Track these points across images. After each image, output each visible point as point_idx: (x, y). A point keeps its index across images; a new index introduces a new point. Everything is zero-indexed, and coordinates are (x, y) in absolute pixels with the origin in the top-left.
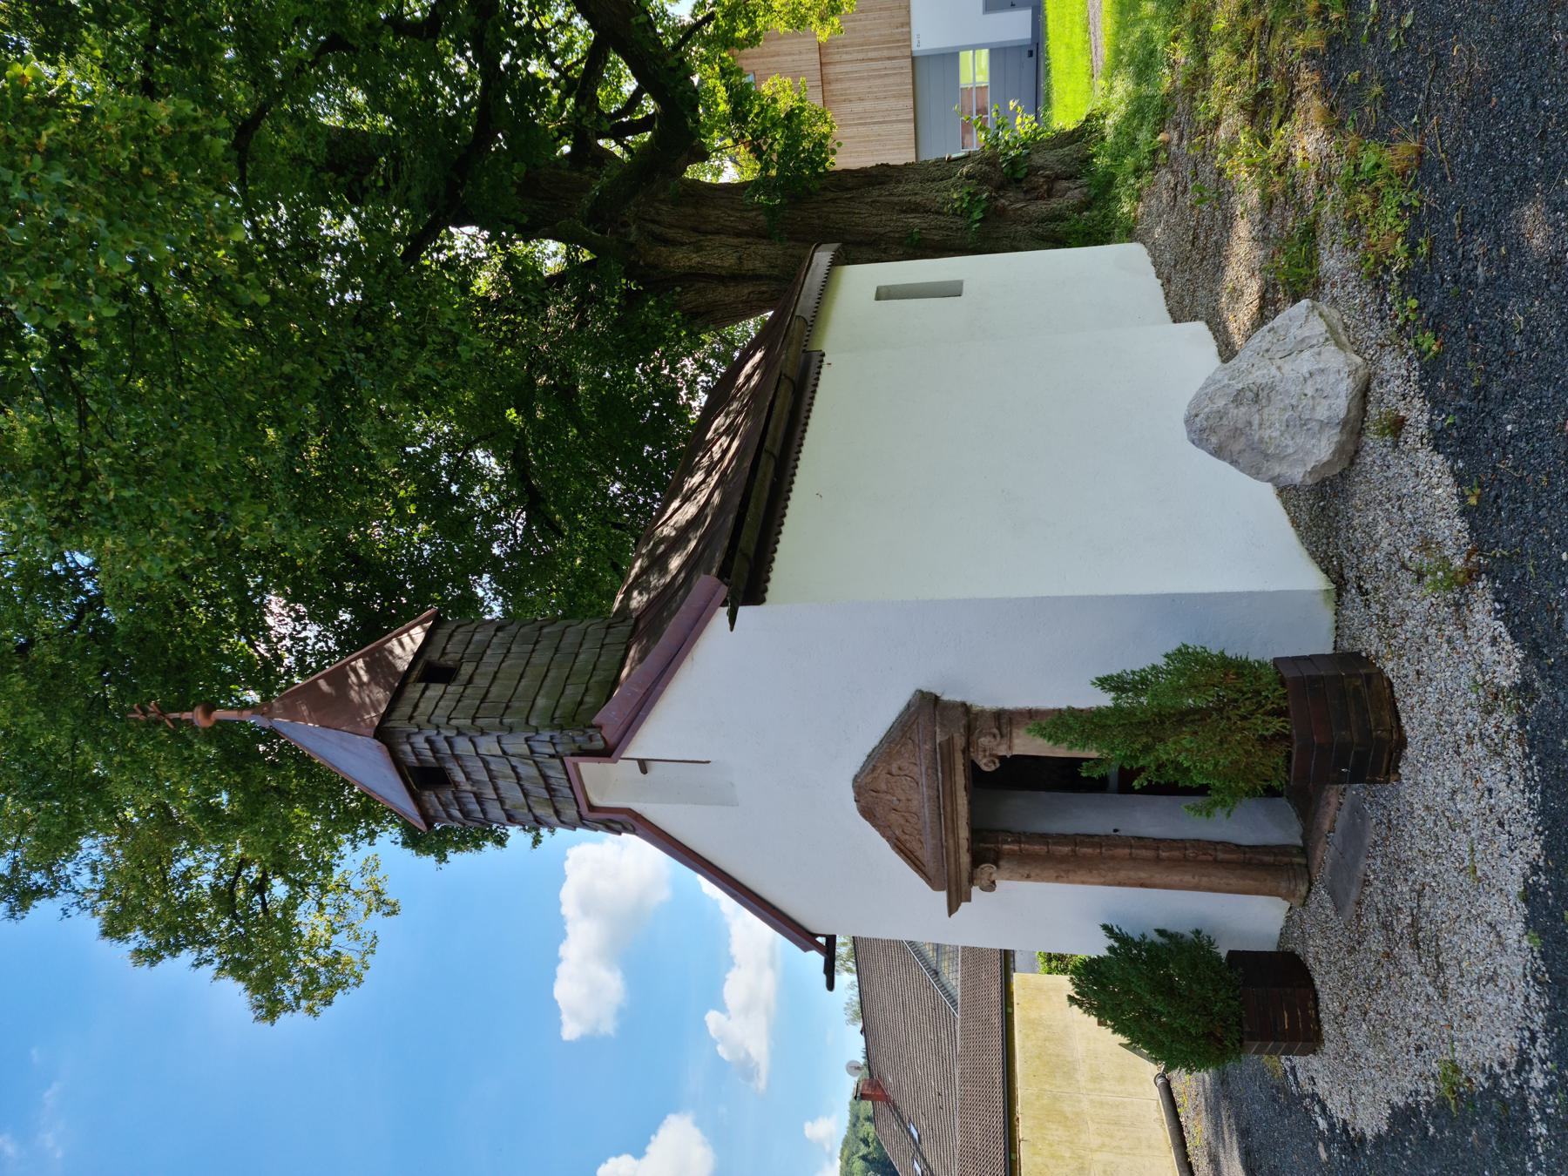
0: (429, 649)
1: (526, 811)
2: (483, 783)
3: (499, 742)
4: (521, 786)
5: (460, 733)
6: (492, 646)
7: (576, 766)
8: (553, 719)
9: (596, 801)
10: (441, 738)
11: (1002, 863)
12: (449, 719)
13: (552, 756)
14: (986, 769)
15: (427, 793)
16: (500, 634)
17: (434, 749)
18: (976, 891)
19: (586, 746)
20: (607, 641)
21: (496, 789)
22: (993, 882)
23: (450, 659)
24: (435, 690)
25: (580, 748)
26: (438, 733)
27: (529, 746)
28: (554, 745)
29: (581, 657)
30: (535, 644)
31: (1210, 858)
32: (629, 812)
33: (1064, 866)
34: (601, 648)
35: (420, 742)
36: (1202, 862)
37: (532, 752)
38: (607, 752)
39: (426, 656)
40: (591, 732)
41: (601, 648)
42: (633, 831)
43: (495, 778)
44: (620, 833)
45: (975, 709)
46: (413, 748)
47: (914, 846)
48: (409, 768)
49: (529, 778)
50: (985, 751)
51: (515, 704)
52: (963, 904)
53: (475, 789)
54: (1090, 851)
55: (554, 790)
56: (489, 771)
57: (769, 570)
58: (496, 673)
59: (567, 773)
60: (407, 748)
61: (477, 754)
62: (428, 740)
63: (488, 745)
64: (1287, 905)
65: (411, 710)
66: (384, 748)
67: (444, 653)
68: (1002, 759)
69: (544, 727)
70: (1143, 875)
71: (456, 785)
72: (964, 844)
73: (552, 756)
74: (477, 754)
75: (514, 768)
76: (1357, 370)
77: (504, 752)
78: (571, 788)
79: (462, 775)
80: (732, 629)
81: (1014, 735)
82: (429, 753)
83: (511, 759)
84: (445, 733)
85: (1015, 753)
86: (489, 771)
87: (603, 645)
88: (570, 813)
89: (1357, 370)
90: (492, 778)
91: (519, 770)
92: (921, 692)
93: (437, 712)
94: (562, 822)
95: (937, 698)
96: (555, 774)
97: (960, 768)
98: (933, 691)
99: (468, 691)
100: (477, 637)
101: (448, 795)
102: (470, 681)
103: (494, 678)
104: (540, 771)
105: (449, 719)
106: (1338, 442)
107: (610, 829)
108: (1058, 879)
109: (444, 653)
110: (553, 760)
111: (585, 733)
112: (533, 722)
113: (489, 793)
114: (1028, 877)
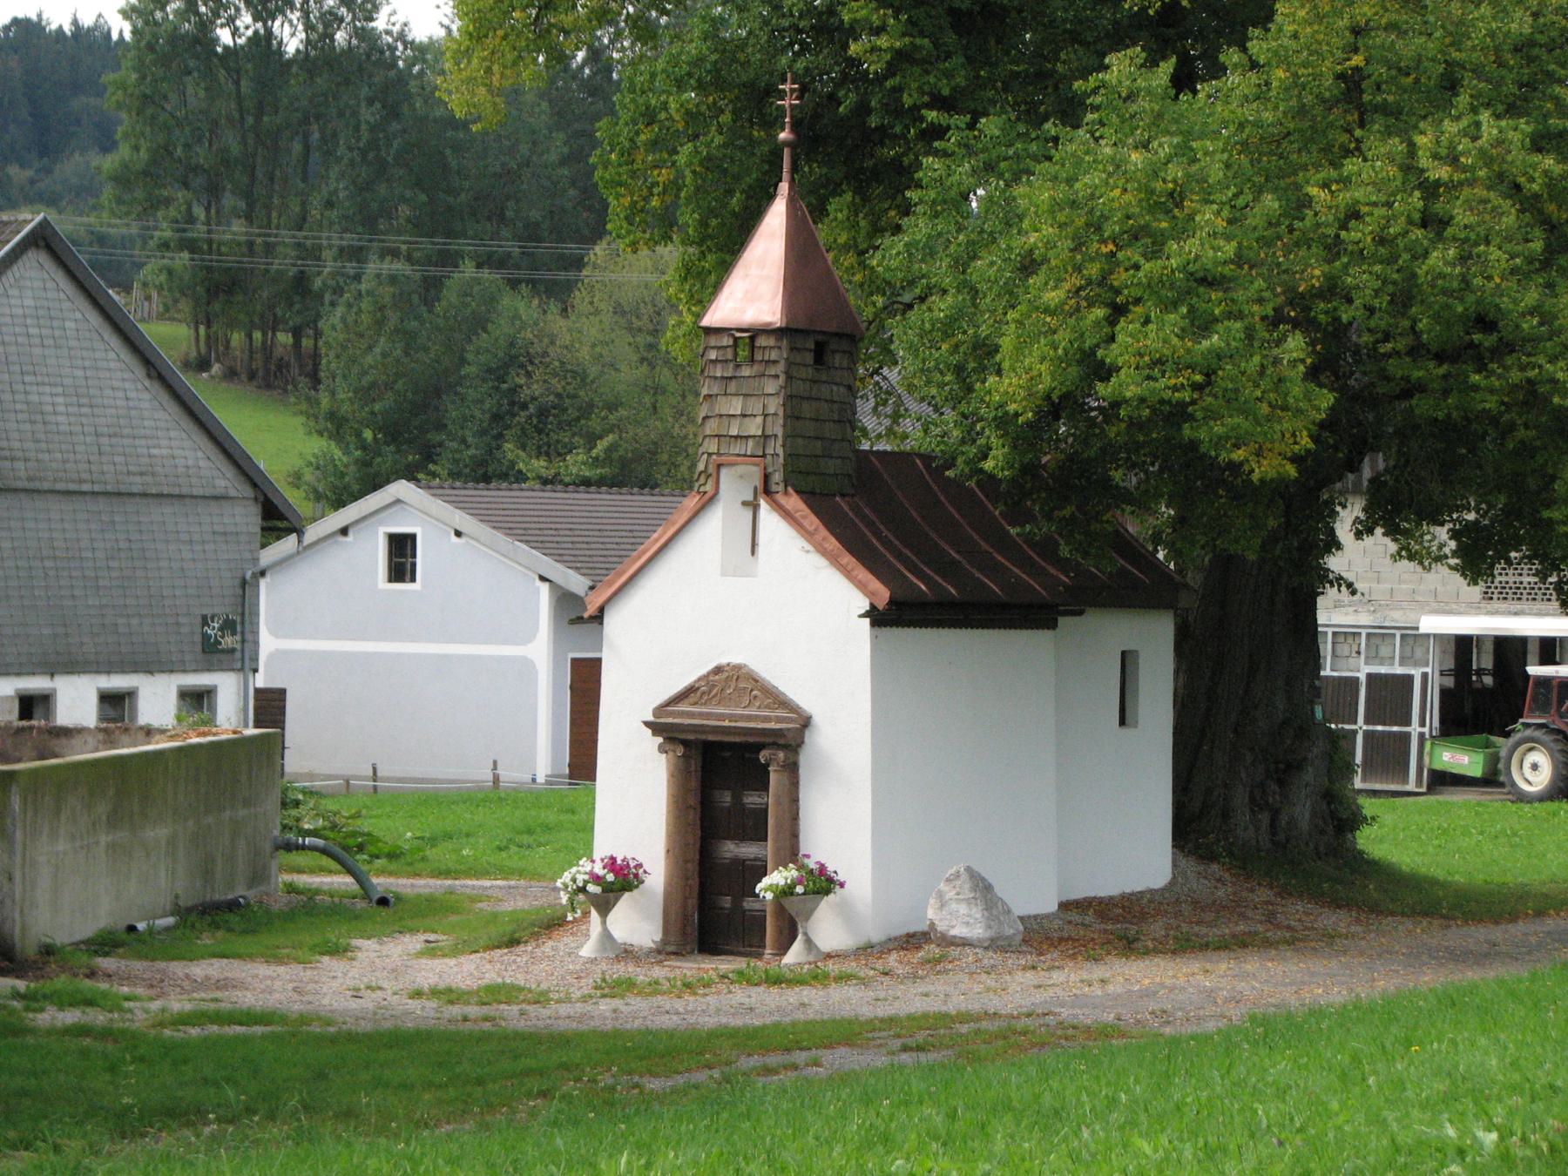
9: (724, 472)
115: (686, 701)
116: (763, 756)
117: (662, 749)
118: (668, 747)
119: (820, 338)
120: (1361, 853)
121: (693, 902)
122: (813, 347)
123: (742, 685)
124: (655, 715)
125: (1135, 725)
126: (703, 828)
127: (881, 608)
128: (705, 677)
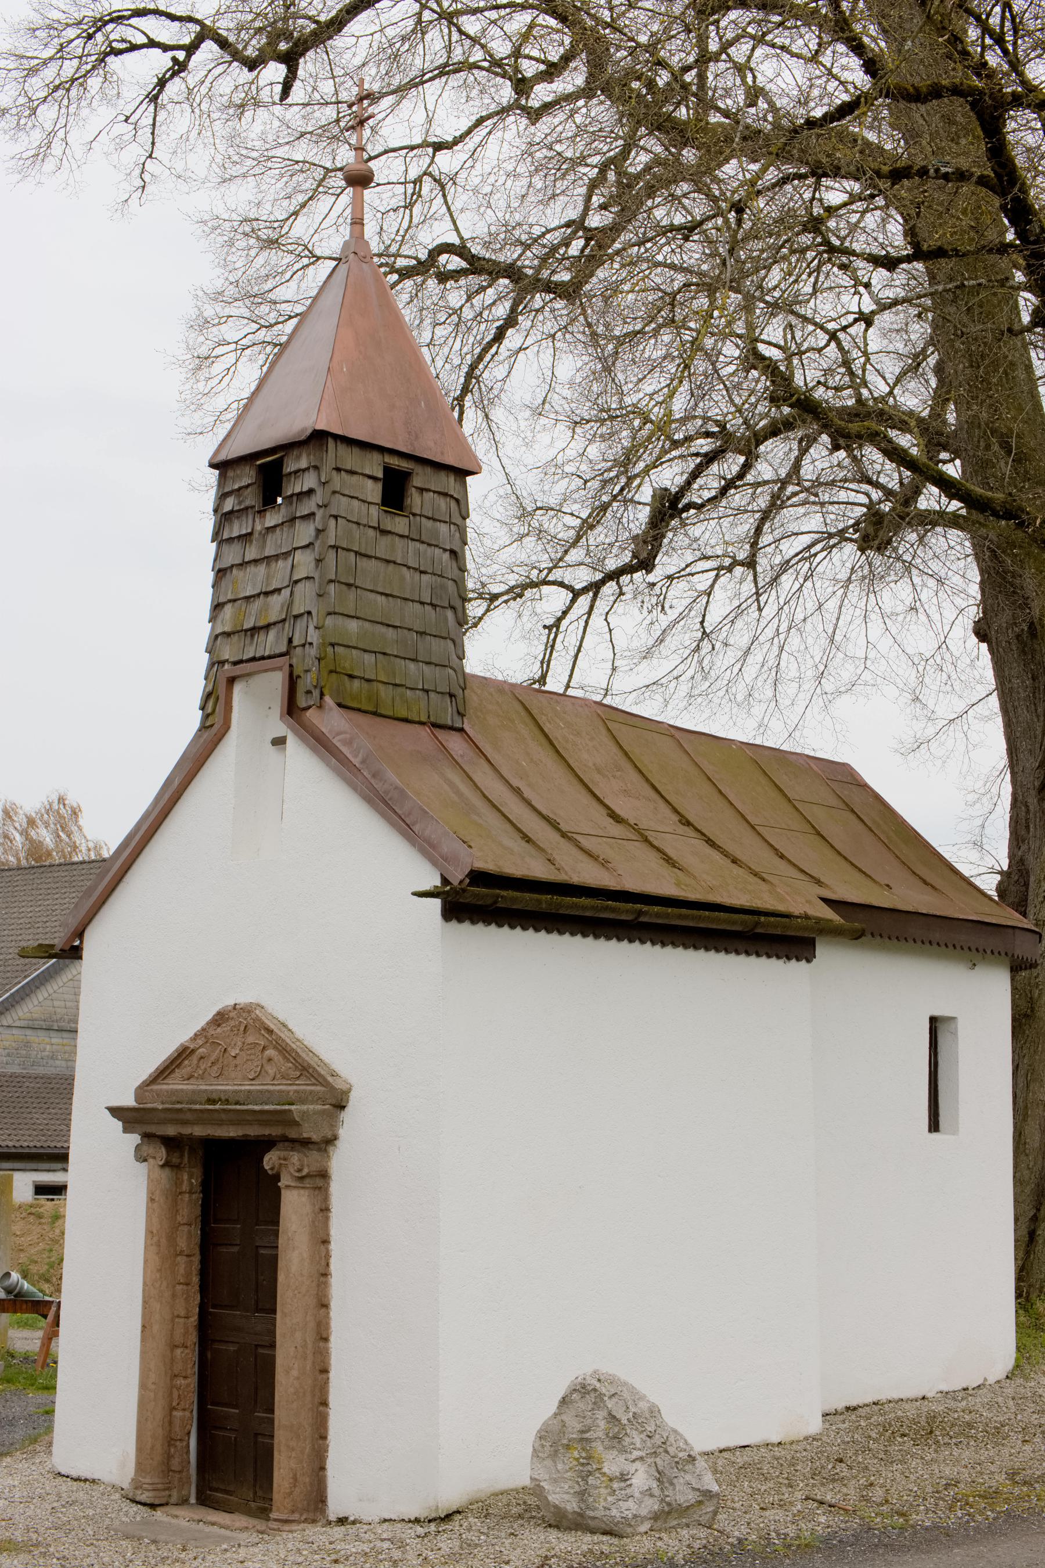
0: (428, 470)
1: (230, 597)
2: (263, 547)
3: (307, 578)
4: (259, 595)
5: (319, 532)
6: (430, 550)
7: (280, 669)
8: (333, 645)
9: (238, 689)
10: (314, 509)
11: (167, 1170)
12: (336, 517)
13: (290, 641)
14: (266, 1159)
15: (253, 473)
16: (446, 556)
17: (301, 495)
18: (135, 1139)
19: (301, 687)
20: (432, 695)
21: (256, 561)
22: (145, 1160)
23: (415, 500)
24: (373, 491)
25: (299, 677)
26: (319, 506)
27: (301, 615)
28: (303, 645)
29: (412, 666)
30: (431, 604)
31: (174, 1404)
32: (226, 727)
33: (164, 1241)
34: (423, 690)
35: (309, 481)
36: (171, 1394)
37: (296, 617)
38: (292, 709)
39: (419, 470)
40: (316, 693)
41: (423, 690)
42: (204, 727)
43: (268, 564)
44: (202, 708)
45: (331, 1149)
46: (304, 470)
47: (185, 1071)
48: (281, 459)
49: (266, 608)
50: (285, 1159)
51: (352, 594)
52: (120, 1123)
53: (256, 535)
54: (182, 1271)
55: (252, 636)
56: (277, 557)
57: (488, 922)
58: (395, 563)
59: (270, 657)
60: (303, 464)
61: (295, 549)
62: (311, 492)
63: (304, 562)
64: (125, 1486)
65: (349, 468)
66: (303, 438)
67: (422, 490)
68: (277, 1177)
69: (323, 637)
70: (156, 1328)
71: (261, 512)
72: (187, 1130)
73: (290, 641)
74: (295, 549)
75: (278, 591)
76: (630, 1525)
77: (296, 582)
78: (253, 659)
79: (272, 524)
80: (414, 894)
81: (302, 1192)
82: (297, 490)
83: (289, 589)
84: (319, 514)
85: (283, 1192)
86: (277, 557)
87: (427, 691)
88: (227, 652)
89: (630, 1525)
90: (268, 559)
91: (275, 596)
92: (350, 1090)
93: (344, 499)
94: (217, 637)
95: (343, 1107)
96: (271, 642)
97: (266, 1131)
98: (350, 1104)
99: (371, 533)
100: (443, 528)
101: (252, 499)
102: (384, 532)
103: (388, 561)
104: (274, 624)
105: (336, 517)
106: (566, 1511)
107: (207, 696)
108: (149, 1233)
109: (422, 490)
110: (285, 642)
111: (315, 687)
112: (329, 621)
113: (252, 553)
114: (151, 1200)
115: (178, 1073)
116: (270, 1160)
117: (141, 1157)
118: (148, 1150)
119: (394, 462)
120: (119, 1120)
121: (188, 1418)
122: (380, 474)
123: (250, 1039)
124: (137, 1099)
125: (955, 1132)
126: (204, 1289)
127: (455, 883)
128: (203, 1032)
